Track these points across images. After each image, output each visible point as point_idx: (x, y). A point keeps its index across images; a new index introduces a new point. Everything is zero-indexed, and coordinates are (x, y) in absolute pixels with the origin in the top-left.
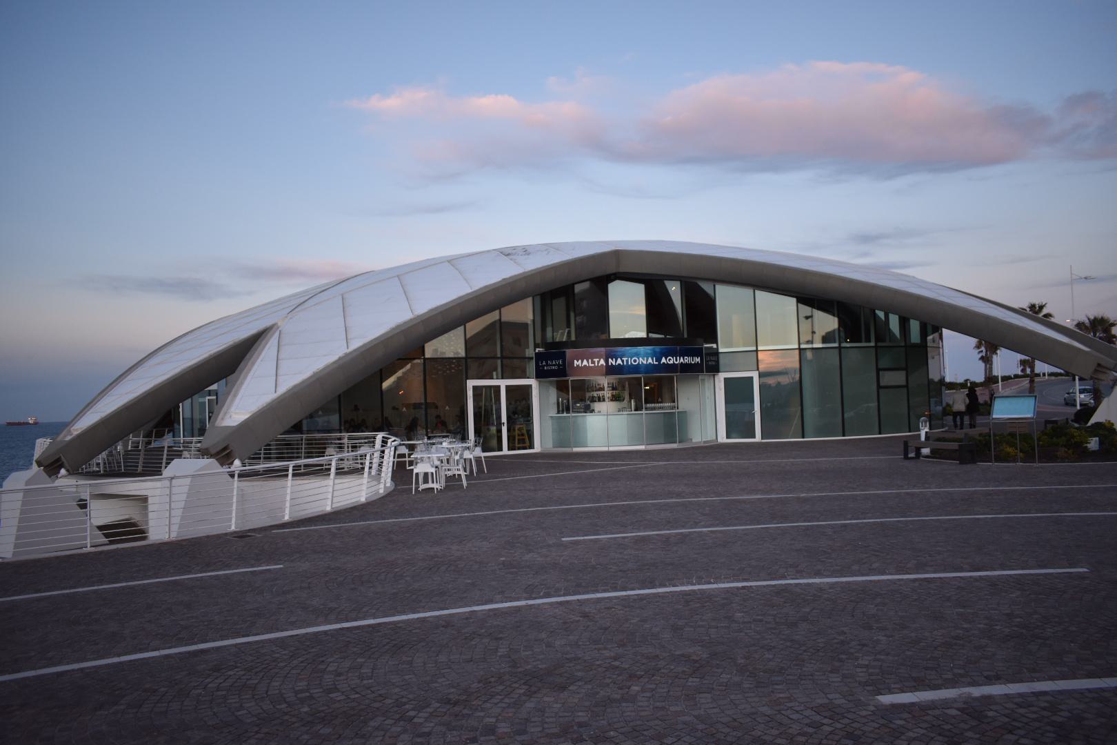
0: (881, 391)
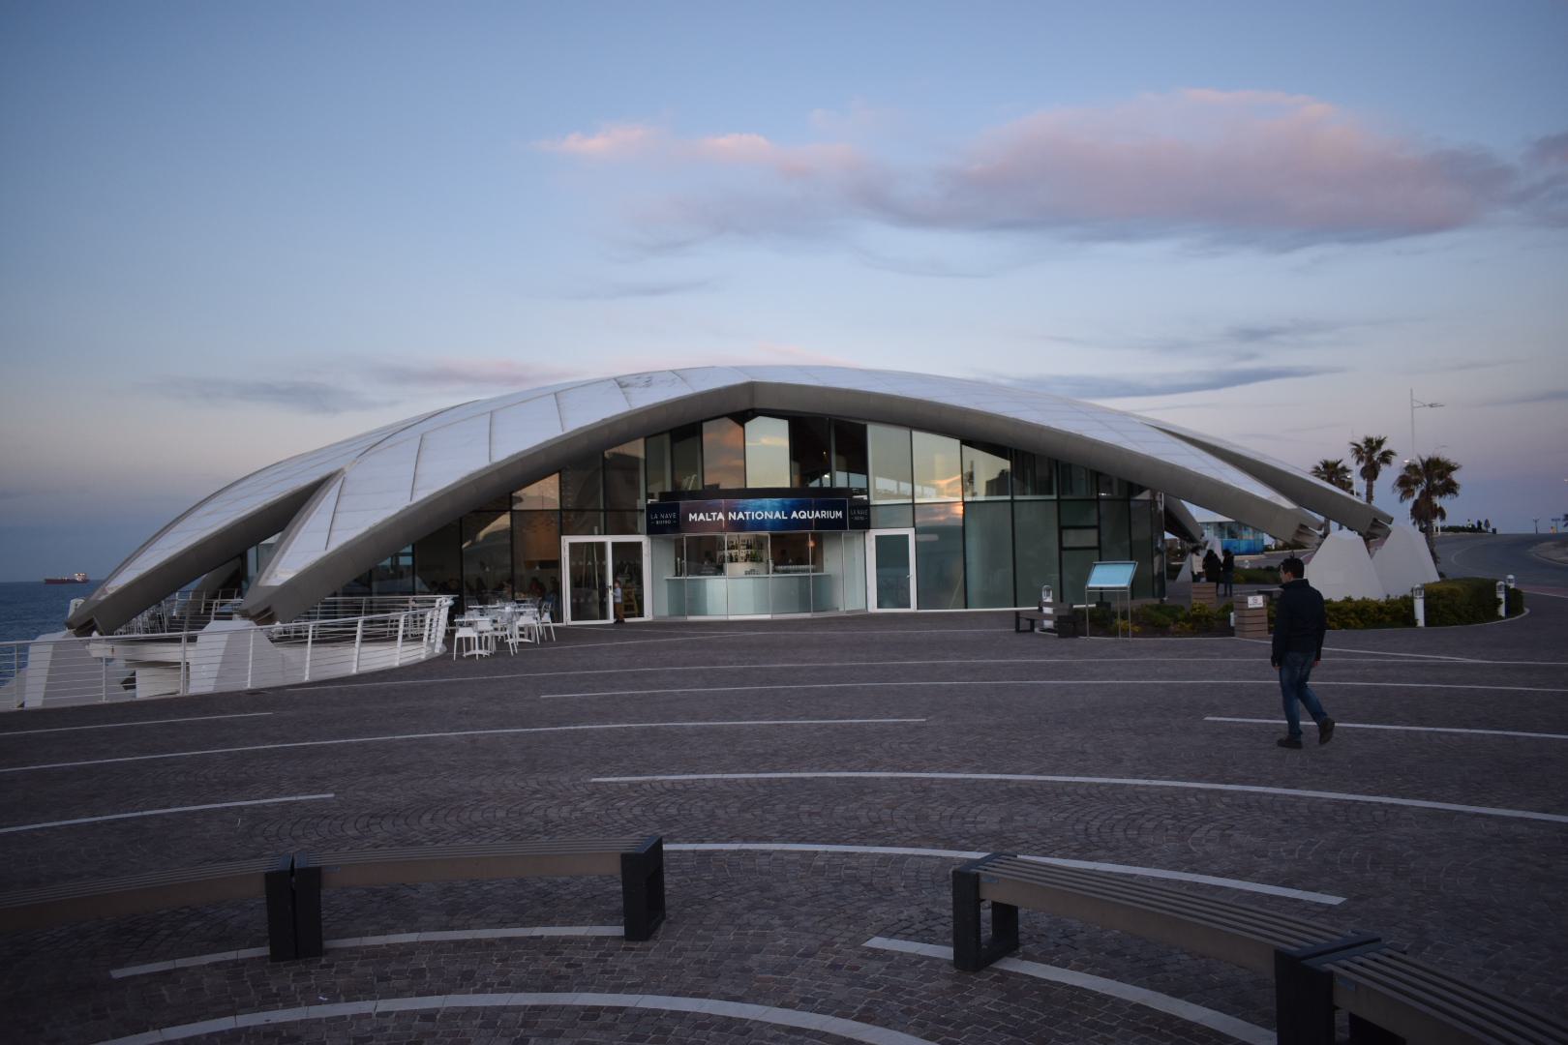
0: (1064, 553)
